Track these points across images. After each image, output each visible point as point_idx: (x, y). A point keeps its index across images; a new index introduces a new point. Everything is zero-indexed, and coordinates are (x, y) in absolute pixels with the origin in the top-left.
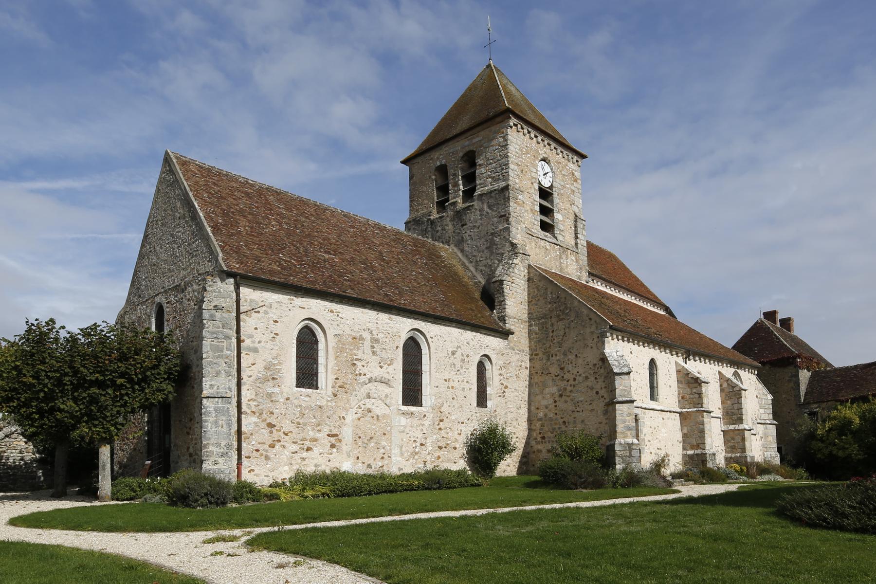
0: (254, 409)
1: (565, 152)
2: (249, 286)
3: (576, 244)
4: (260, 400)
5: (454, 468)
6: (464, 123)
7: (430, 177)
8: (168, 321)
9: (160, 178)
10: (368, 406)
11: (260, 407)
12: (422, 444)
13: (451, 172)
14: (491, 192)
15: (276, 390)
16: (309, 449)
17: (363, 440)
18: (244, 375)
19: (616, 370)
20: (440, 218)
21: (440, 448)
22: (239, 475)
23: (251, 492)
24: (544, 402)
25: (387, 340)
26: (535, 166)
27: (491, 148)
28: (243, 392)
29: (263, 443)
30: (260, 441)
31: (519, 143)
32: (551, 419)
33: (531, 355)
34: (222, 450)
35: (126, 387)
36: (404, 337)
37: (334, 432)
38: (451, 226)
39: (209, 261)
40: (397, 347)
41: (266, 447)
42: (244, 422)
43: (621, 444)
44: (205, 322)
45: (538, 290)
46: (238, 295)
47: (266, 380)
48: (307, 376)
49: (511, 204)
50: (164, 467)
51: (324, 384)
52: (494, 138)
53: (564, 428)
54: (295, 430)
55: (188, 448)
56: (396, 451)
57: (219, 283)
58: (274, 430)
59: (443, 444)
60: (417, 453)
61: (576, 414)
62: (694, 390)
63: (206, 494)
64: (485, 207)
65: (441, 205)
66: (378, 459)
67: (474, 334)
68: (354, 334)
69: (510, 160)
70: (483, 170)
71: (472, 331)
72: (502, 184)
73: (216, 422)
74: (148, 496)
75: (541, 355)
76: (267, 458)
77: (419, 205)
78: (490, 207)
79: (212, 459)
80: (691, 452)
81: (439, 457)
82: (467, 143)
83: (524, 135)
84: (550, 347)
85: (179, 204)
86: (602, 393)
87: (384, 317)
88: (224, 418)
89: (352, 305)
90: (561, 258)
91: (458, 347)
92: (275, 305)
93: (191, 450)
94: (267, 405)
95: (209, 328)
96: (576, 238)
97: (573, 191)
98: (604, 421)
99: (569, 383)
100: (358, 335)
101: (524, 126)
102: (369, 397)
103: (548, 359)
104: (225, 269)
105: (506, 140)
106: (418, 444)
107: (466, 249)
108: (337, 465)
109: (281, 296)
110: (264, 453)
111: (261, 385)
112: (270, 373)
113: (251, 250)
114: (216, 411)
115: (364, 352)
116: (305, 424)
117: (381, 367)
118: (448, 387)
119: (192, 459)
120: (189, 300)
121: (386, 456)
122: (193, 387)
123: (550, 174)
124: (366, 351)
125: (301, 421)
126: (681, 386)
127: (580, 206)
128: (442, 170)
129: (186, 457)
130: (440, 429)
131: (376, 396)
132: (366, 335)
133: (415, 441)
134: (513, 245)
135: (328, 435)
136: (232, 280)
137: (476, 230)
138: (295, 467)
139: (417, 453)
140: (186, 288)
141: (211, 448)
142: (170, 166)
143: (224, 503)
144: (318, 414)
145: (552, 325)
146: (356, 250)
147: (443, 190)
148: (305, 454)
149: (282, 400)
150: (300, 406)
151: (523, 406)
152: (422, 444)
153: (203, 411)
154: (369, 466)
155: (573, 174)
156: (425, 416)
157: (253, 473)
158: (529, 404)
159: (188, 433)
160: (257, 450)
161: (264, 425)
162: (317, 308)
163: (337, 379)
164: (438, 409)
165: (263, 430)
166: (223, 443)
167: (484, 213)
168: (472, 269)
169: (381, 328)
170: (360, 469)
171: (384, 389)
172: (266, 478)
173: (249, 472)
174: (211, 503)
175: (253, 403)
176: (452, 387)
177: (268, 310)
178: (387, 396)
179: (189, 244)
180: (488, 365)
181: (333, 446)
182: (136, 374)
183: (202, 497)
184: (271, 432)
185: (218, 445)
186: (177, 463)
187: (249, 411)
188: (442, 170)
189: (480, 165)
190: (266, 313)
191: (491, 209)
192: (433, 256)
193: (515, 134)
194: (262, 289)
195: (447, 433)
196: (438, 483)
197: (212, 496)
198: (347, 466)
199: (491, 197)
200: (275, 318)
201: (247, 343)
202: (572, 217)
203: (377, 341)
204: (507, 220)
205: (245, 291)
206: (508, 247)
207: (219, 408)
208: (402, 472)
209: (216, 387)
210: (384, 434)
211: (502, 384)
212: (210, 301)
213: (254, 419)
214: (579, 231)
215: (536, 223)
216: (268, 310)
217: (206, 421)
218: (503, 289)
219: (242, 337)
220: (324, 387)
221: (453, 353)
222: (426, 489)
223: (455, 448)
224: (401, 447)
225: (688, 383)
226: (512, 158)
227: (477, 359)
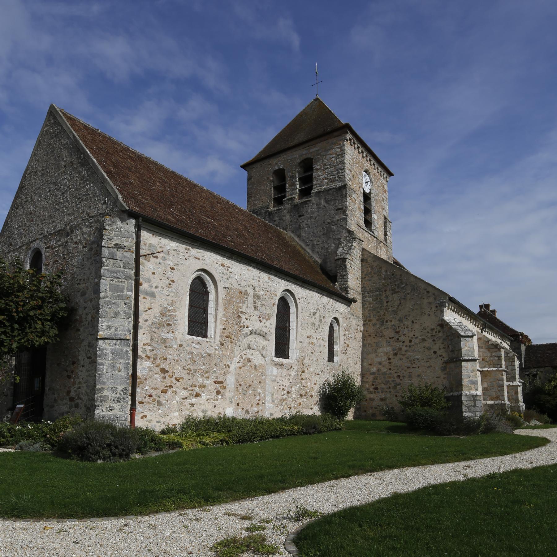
0: (148, 354)
1: (379, 169)
2: (149, 230)
3: (386, 239)
4: (155, 345)
5: (310, 413)
6: (301, 137)
7: (268, 178)
8: (46, 265)
9: (43, 130)
10: (249, 356)
11: (155, 352)
12: (288, 392)
13: (288, 174)
14: (329, 190)
15: (170, 336)
16: (197, 395)
17: (244, 387)
18: (141, 320)
19: (462, 334)
20: (278, 210)
21: (301, 396)
22: (132, 421)
23: (152, 440)
24: (379, 360)
25: (266, 297)
26: (361, 174)
27: (328, 157)
28: (140, 336)
29: (156, 389)
30: (153, 386)
31: (352, 154)
32: (384, 373)
33: (364, 321)
34: (118, 395)
35: (5, 326)
36: (279, 294)
37: (220, 380)
38: (288, 217)
39: (104, 203)
40: (274, 305)
41: (159, 392)
42: (139, 367)
43: (466, 395)
44: (104, 260)
45: (372, 269)
46: (138, 237)
47: (161, 325)
48: (198, 325)
49: (348, 199)
50: (35, 412)
51: (213, 331)
52: (331, 149)
53: (398, 381)
54: (186, 377)
55: (68, 392)
56: (268, 398)
57: (119, 223)
58: (167, 375)
59: (303, 392)
60: (284, 400)
61: (412, 370)
62: (494, 354)
63: (109, 445)
64: (322, 202)
65: (279, 201)
66: (255, 405)
67: (329, 299)
68: (240, 289)
69: (346, 166)
70: (320, 173)
71: (327, 296)
72: (340, 184)
73: (113, 366)
74: (23, 443)
75: (374, 321)
76: (159, 404)
77: (256, 200)
78: (327, 202)
79: (106, 405)
80: (491, 402)
81: (300, 404)
82: (305, 152)
83: (355, 148)
84: (384, 314)
85: (65, 153)
86: (439, 352)
87: (264, 276)
88: (122, 361)
89: (239, 262)
90: (377, 248)
91: (318, 309)
92: (172, 252)
93: (73, 394)
94: (161, 351)
95: (108, 266)
96: (386, 234)
97: (383, 199)
98: (442, 376)
99: (405, 344)
100: (244, 290)
101: (356, 142)
102: (249, 348)
103: (382, 324)
104: (128, 208)
105: (343, 150)
106: (286, 392)
107: (303, 234)
108: (222, 411)
109: (178, 244)
110: (157, 399)
111: (156, 330)
112: (165, 319)
113: (146, 199)
114: (113, 354)
115: (247, 306)
116: (195, 371)
117: (261, 321)
118: (309, 343)
119: (73, 403)
120: (76, 243)
121: (261, 403)
122: (79, 330)
123: (369, 183)
124: (249, 306)
125: (192, 368)
126: (481, 350)
127: (388, 211)
128: (280, 175)
129: (64, 401)
130: (302, 379)
131: (255, 347)
132: (250, 291)
133: (283, 389)
134: (350, 233)
135: (215, 382)
136: (133, 221)
137: (313, 220)
138: (186, 413)
139: (284, 400)
140: (72, 232)
141: (106, 393)
142: (55, 118)
143: (127, 455)
144: (207, 361)
145: (387, 297)
146: (226, 220)
147: (280, 189)
148: (194, 400)
149: (175, 346)
150: (192, 353)
151: (358, 362)
152: (288, 392)
153: (99, 353)
154: (247, 412)
155: (383, 187)
156: (292, 367)
157: (145, 419)
158: (362, 361)
159: (69, 377)
160: (150, 396)
161: (157, 370)
162: (211, 260)
163: (224, 329)
164: (300, 361)
165: (157, 376)
166: (120, 388)
167: (322, 206)
168: (309, 251)
169: (262, 286)
170: (240, 415)
171: (261, 342)
172: (158, 424)
173: (142, 418)
174: (114, 455)
175: (148, 348)
176: (312, 343)
177: (166, 256)
178: (263, 348)
179: (77, 190)
180: (336, 327)
181: (218, 393)
182: (17, 312)
183: (104, 448)
184: (164, 378)
185: (114, 390)
186: (53, 406)
187: (144, 356)
188: (280, 175)
189: (317, 169)
190: (164, 259)
191: (328, 204)
192: (279, 236)
193: (349, 146)
194: (161, 235)
195: (307, 383)
196: (314, 428)
197: (116, 447)
198: (229, 412)
199: (329, 194)
200: (172, 265)
201: (145, 286)
202: (383, 218)
203: (258, 297)
204: (344, 212)
205: (145, 235)
206: (345, 233)
207: (117, 350)
208: (272, 417)
209: (113, 329)
210: (260, 382)
211: (345, 343)
212: (109, 240)
213: (148, 364)
214: (388, 229)
215: (361, 218)
216: (166, 256)
217: (101, 364)
218: (345, 266)
219: (141, 281)
220: (213, 336)
221: (314, 314)
222: (305, 433)
223: (312, 396)
224: (273, 395)
225: (489, 348)
226: (347, 165)
227: (329, 320)
